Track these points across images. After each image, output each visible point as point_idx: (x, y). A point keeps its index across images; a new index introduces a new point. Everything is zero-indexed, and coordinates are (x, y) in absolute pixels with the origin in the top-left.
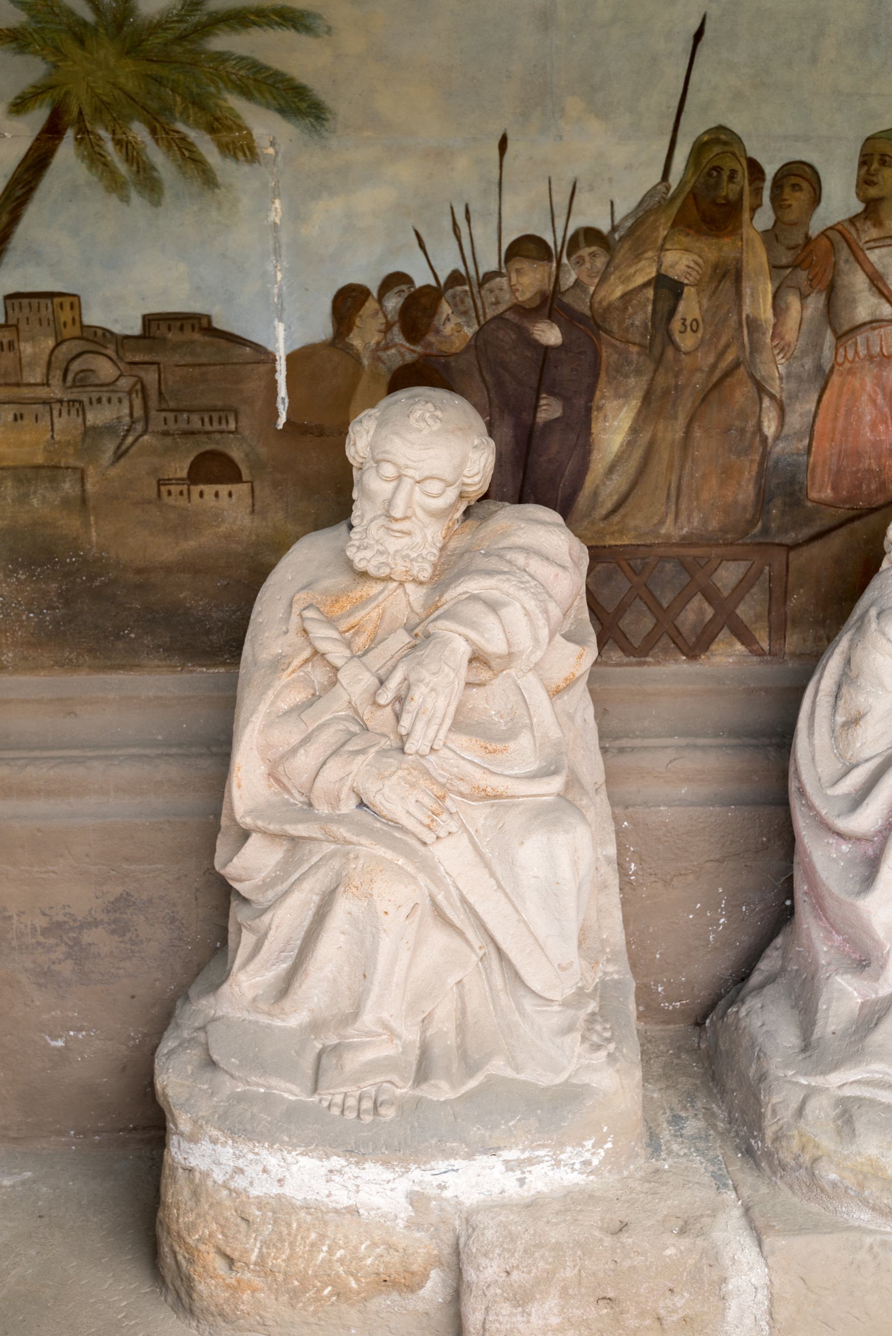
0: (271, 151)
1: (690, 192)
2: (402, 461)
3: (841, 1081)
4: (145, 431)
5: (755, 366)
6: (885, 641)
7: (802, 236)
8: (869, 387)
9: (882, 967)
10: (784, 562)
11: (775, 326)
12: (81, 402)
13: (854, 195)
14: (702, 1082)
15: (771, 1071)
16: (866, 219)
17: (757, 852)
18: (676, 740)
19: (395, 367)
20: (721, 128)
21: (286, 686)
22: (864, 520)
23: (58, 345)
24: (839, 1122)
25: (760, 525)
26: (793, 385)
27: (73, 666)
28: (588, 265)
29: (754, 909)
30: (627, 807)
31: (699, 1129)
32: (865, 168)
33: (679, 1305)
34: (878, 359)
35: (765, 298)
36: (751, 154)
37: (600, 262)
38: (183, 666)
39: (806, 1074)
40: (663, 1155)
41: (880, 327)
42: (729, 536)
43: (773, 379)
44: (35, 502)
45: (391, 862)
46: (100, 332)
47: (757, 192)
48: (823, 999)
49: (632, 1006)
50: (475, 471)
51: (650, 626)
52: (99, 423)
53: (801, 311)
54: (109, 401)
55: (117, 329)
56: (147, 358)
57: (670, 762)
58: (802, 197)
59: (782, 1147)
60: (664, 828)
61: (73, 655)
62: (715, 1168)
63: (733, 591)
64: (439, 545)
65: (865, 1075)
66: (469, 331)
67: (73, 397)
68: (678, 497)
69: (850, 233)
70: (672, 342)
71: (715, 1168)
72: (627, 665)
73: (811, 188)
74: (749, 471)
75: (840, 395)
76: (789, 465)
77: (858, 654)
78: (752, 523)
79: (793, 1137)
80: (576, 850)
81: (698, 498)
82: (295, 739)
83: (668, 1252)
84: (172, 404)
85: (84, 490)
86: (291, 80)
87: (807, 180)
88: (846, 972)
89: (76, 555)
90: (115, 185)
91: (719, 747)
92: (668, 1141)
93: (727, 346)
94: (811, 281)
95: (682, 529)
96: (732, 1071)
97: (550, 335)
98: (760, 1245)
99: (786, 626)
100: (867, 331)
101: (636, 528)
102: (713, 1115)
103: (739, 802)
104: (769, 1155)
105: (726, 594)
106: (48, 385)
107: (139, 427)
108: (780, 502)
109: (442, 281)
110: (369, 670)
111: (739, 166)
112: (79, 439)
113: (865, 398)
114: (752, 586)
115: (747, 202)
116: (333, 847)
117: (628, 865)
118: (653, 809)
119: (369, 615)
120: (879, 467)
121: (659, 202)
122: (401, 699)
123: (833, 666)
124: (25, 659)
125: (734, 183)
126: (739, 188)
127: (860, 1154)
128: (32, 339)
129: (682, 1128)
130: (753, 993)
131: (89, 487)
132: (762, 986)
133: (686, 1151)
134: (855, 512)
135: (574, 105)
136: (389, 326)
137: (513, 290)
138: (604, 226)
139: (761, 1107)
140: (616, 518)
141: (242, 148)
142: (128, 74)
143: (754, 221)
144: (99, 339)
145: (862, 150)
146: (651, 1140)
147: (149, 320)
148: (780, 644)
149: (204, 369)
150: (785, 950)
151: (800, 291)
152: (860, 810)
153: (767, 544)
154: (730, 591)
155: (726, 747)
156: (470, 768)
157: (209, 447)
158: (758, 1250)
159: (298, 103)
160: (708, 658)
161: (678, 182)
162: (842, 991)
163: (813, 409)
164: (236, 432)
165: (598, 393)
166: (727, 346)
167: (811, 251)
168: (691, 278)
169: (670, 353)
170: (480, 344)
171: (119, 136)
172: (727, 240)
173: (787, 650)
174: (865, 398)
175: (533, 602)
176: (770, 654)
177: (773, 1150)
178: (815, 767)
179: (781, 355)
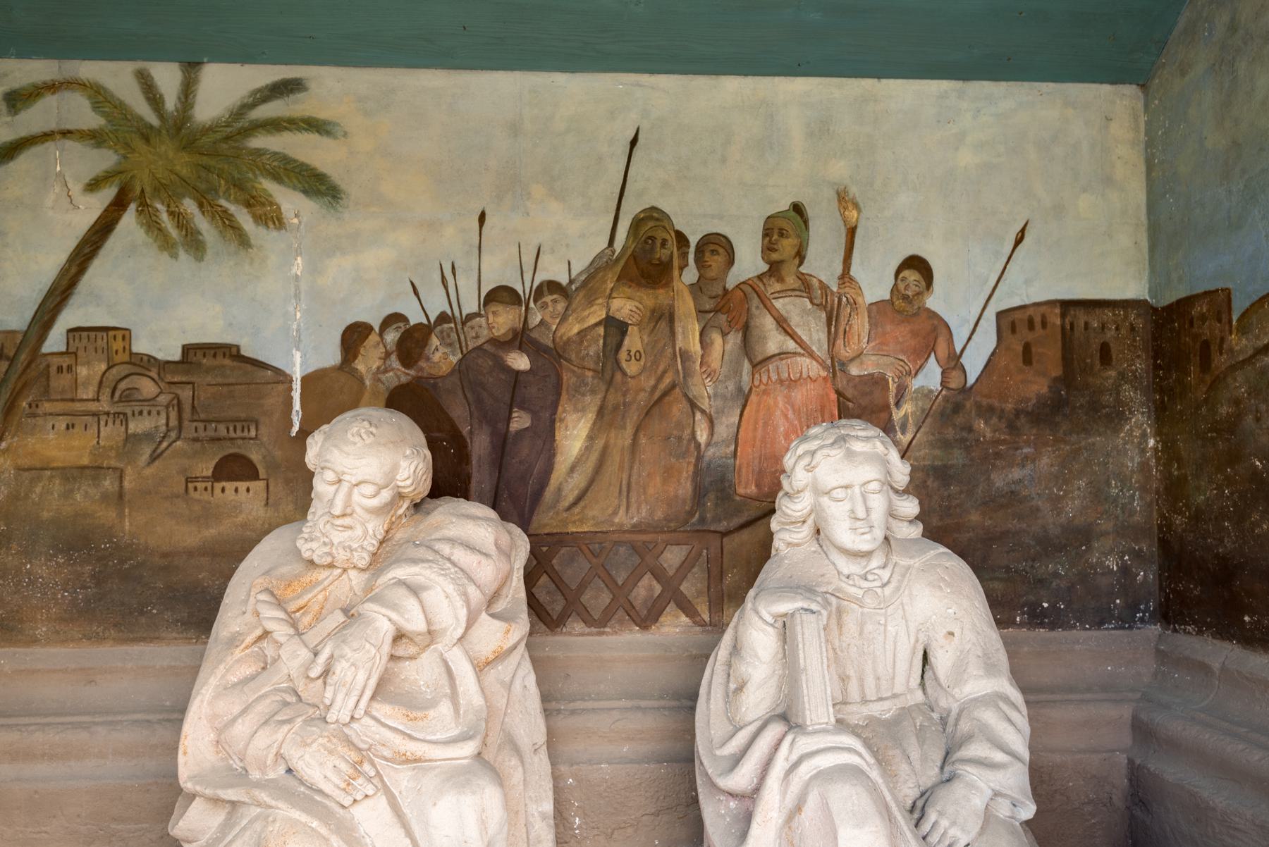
0: (296, 221)
2: (339, 468)
4: (178, 438)
11: (702, 356)
12: (125, 414)
19: (392, 386)
20: (653, 209)
21: (238, 661)
23: (109, 368)
26: (719, 403)
27: (99, 639)
28: (551, 309)
36: (677, 227)
37: (561, 306)
38: (198, 638)
44: (78, 497)
45: (305, 825)
46: (145, 358)
47: (684, 256)
50: (406, 476)
51: (608, 601)
52: (139, 431)
53: (723, 346)
54: (149, 413)
55: (160, 356)
56: (184, 379)
61: (100, 630)
63: (677, 570)
64: (380, 537)
66: (454, 359)
67: (119, 410)
68: (628, 492)
70: (621, 369)
72: (588, 634)
74: (687, 471)
75: (758, 411)
77: (741, 628)
78: (691, 514)
80: (483, 811)
81: (645, 493)
82: (237, 709)
84: (203, 416)
85: (121, 487)
86: (314, 169)
89: (110, 542)
90: (167, 245)
93: (664, 372)
97: (520, 362)
101: (594, 518)
105: (671, 573)
106: (98, 400)
107: (173, 435)
109: (432, 321)
110: (306, 646)
112: (120, 444)
113: (778, 413)
114: (693, 567)
115: (676, 263)
116: (259, 810)
119: (314, 598)
122: (326, 673)
124: (58, 632)
128: (88, 363)
131: (126, 484)
135: (538, 190)
136: (388, 355)
137: (490, 328)
138: (564, 280)
140: (577, 510)
141: (272, 218)
142: (183, 164)
144: (144, 364)
147: (187, 349)
149: (232, 388)
156: (389, 734)
157: (232, 451)
159: (318, 185)
164: (256, 438)
165: (560, 408)
166: (664, 372)
169: (618, 376)
170: (462, 369)
171: (172, 209)
172: (661, 291)
174: (778, 413)
175: (451, 586)
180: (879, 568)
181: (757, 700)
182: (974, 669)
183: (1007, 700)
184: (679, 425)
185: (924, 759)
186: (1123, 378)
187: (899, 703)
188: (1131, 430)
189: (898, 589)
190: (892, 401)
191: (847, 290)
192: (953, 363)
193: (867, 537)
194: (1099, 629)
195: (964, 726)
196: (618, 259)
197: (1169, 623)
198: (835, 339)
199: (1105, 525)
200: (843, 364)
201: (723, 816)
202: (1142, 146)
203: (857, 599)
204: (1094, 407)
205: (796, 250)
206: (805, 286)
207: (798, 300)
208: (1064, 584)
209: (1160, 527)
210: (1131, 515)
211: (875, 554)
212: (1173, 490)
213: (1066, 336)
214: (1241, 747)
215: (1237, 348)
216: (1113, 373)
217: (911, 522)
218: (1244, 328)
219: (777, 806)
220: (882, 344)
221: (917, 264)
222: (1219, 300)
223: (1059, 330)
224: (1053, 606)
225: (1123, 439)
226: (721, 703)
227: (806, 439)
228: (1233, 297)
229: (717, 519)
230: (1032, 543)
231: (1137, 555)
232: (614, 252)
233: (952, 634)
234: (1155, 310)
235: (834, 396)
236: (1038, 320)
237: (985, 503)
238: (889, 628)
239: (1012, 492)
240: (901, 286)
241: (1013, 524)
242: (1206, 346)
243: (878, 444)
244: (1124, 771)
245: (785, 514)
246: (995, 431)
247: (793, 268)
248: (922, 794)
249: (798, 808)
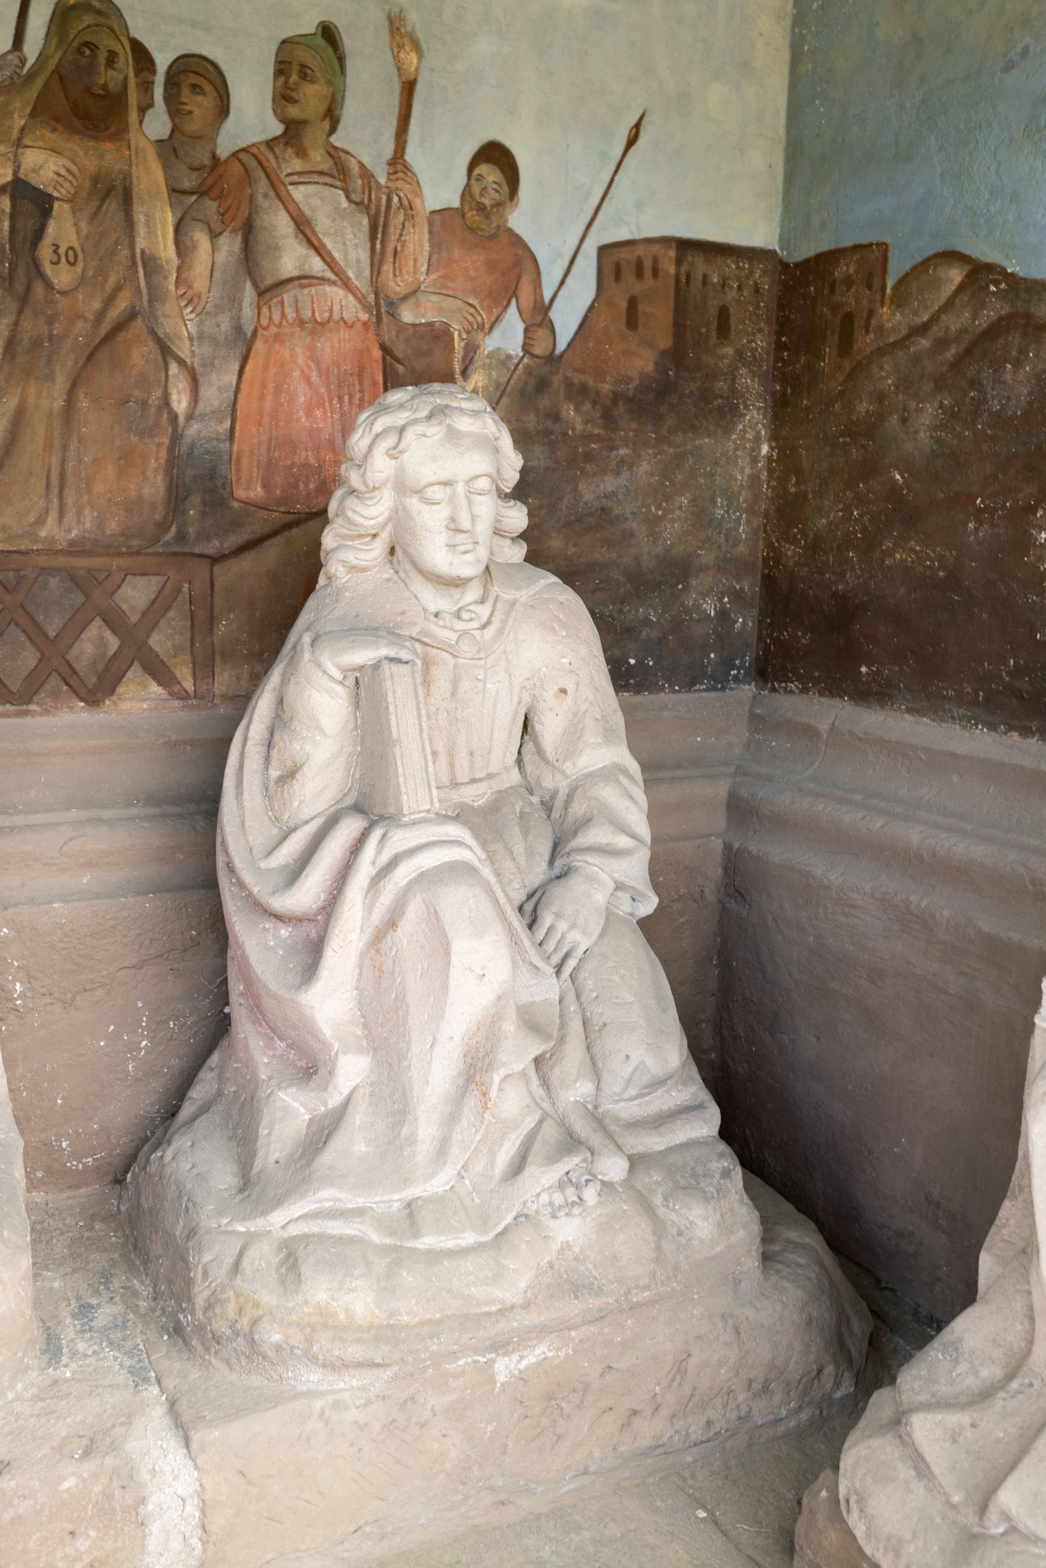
1: (53, 72)
3: (285, 1219)
5: (156, 319)
6: (320, 674)
7: (208, 154)
8: (300, 360)
9: (331, 1073)
10: (208, 578)
11: (179, 269)
13: (271, 111)
14: (121, 1255)
15: (202, 1224)
16: (286, 144)
17: (185, 950)
18: (74, 814)
22: (303, 527)
24: (283, 1270)
25: (173, 529)
26: (206, 349)
29: (185, 1024)
30: (6, 908)
31: (115, 1316)
32: (282, 79)
33: (83, 1549)
34: (310, 325)
35: (164, 228)
36: (135, 34)
39: (243, 1219)
40: (64, 1360)
41: (311, 285)
42: (134, 543)
43: (180, 338)
47: (147, 87)
48: (264, 1122)
49: (19, 1173)
51: (33, 663)
53: (212, 255)
57: (66, 843)
58: (206, 103)
59: (216, 1315)
60: (59, 931)
62: (133, 1362)
63: (144, 614)
65: (313, 1207)
69: (268, 161)
70: (42, 276)
71: (133, 1362)
73: (215, 94)
74: (156, 459)
75: (266, 368)
76: (208, 452)
77: (291, 690)
78: (163, 526)
79: (228, 1300)
81: (89, 490)
83: (66, 1485)
87: (210, 82)
88: (290, 1085)
91: (131, 819)
92: (72, 1340)
93: (118, 289)
94: (223, 215)
95: (69, 531)
96: (157, 1233)
98: (187, 1446)
99: (214, 660)
100: (294, 288)
102: (135, 1294)
103: (158, 889)
104: (200, 1329)
105: (134, 618)
108: (198, 500)
111: (120, 47)
113: (296, 373)
114: (168, 609)
115: (133, 98)
117: (10, 986)
118: (43, 907)
120: (318, 462)
121: (11, 78)
123: (263, 706)
125: (114, 69)
126: (121, 78)
127: (306, 1303)
129: (91, 1320)
130: (182, 1130)
132: (193, 1119)
133: (95, 1348)
134: (292, 517)
139: (189, 1270)
143: (144, 126)
145: (277, 55)
146: (48, 1344)
148: (208, 684)
150: (222, 1069)
151: (209, 226)
152: (297, 885)
153: (185, 554)
154: (139, 616)
155: (141, 818)
158: (185, 1451)
160: (115, 704)
161: (36, 55)
162: (287, 1109)
163: (234, 383)
166: (118, 289)
167: (221, 175)
168: (62, 190)
169: (39, 289)
172: (108, 145)
173: (217, 692)
174: (296, 373)
176: (195, 697)
177: (205, 1321)
178: (245, 835)
179: (190, 309)
180: (475, 602)
181: (317, 789)
182: (592, 735)
183: (625, 772)
184: (143, 382)
185: (530, 853)
186: (741, 357)
187: (495, 785)
188: (744, 431)
189: (501, 631)
190: (457, 368)
191: (400, 184)
192: (539, 318)
193: (469, 557)
194: (689, 691)
195: (578, 809)
196: (32, 75)
197: (766, 682)
198: (381, 262)
199: (706, 557)
200: (391, 304)
201: (272, 948)
202: (789, 21)
203: (450, 646)
204: (706, 396)
205: (326, 106)
206: (339, 170)
207: (328, 191)
208: (655, 634)
209: (766, 560)
210: (734, 545)
211: (471, 584)
212: (786, 512)
213: (681, 288)
214: (860, 815)
215: (888, 325)
216: (729, 351)
217: (513, 539)
218: (899, 300)
219: (358, 924)
220: (445, 277)
221: (495, 155)
222: (872, 257)
223: (672, 281)
224: (641, 662)
225: (734, 442)
226: (258, 798)
227: (386, 409)
228: (890, 255)
229: (204, 537)
230: (622, 579)
231: (738, 596)
232: (23, 61)
233: (564, 691)
234: (785, 266)
235: (377, 354)
236: (648, 264)
237: (569, 524)
238: (489, 685)
239: (603, 509)
240: (476, 189)
241: (602, 554)
242: (849, 319)
243: (490, 421)
244: (719, 859)
245: (350, 522)
246: (587, 422)
247: (321, 137)
248: (530, 896)
249: (391, 923)
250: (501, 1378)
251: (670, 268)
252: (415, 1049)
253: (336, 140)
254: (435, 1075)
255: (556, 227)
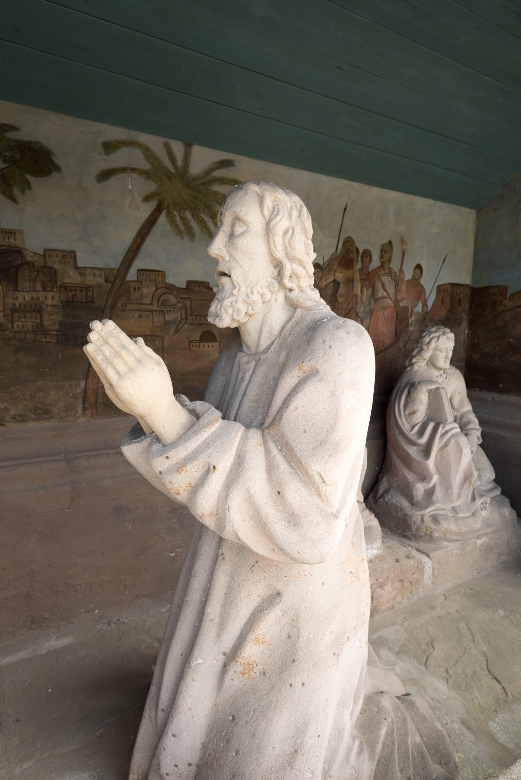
36: (357, 246)
47: (358, 257)
53: (367, 293)
93: (350, 302)
113: (380, 319)
115: (355, 260)
166: (350, 302)
169: (336, 304)
181: (420, 417)
190: (409, 315)
192: (425, 304)
200: (398, 302)
206: (390, 273)
216: (460, 309)
221: (419, 267)
222: (502, 290)
235: (395, 313)
236: (446, 289)
240: (415, 275)
249: (446, 445)
250: (478, 545)
251: (450, 290)
252: (452, 473)
253: (390, 266)
254: (457, 479)
255: (429, 283)
